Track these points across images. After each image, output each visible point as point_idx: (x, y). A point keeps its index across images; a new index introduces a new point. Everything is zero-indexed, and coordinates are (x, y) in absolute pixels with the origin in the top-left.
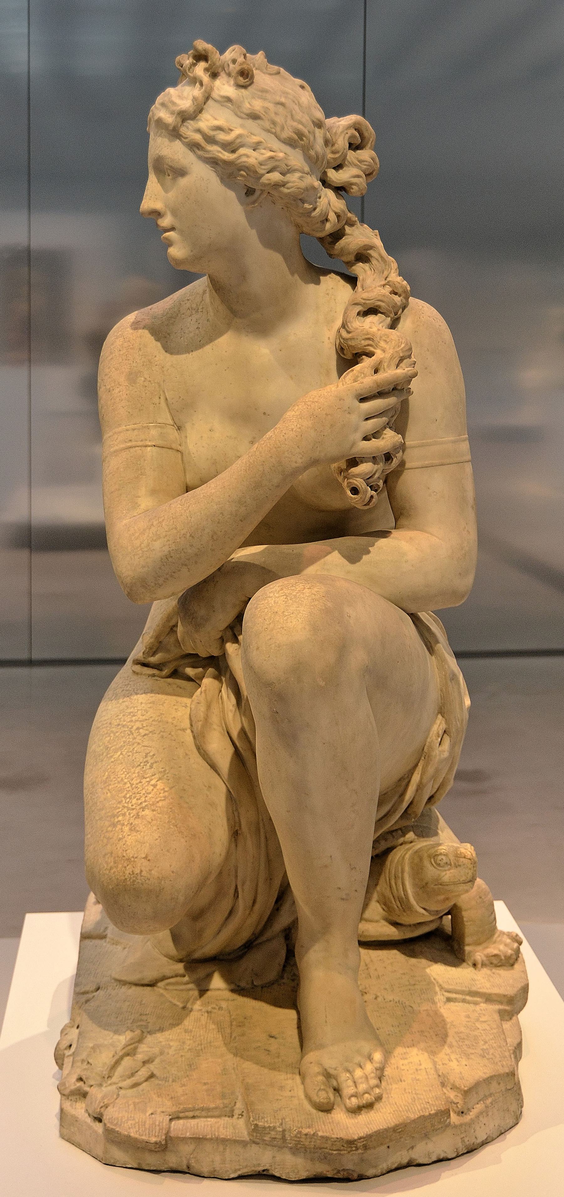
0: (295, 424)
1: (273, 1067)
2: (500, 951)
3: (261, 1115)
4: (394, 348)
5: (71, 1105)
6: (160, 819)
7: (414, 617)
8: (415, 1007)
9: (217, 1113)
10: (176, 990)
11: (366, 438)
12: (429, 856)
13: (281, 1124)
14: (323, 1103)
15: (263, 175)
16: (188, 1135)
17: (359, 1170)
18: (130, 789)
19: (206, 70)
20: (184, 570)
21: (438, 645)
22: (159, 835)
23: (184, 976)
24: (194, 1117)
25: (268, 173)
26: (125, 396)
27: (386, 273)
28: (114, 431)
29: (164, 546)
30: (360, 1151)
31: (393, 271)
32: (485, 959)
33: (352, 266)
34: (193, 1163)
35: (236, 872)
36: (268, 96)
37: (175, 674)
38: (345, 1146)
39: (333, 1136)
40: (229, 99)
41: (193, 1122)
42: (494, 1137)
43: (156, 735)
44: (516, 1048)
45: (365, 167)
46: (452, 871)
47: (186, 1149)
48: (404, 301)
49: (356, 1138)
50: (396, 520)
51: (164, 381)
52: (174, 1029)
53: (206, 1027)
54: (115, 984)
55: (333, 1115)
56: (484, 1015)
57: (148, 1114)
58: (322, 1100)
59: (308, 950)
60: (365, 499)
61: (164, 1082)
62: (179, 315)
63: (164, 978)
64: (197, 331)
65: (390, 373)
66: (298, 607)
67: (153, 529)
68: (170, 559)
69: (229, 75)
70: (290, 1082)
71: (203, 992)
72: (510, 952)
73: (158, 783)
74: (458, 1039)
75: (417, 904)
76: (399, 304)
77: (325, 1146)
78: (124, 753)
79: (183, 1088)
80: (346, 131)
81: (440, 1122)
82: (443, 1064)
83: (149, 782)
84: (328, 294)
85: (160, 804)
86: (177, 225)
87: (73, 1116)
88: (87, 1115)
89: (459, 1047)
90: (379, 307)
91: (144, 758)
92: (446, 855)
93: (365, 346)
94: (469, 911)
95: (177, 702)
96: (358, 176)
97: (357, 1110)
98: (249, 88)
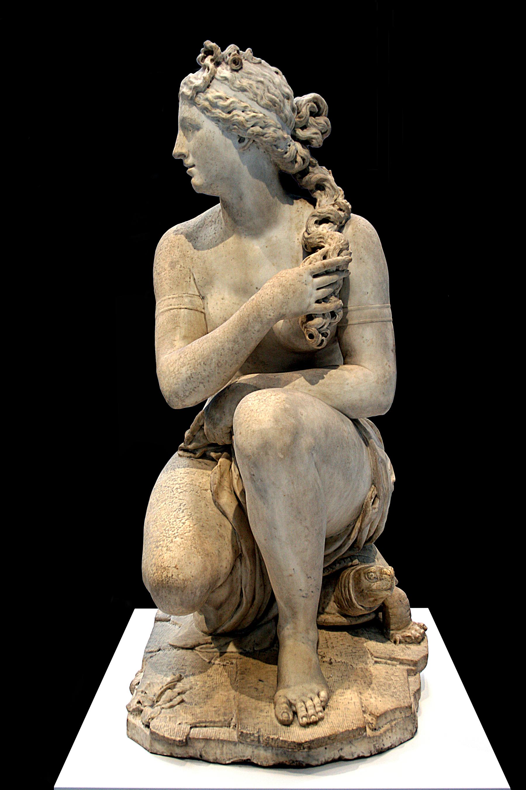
0: (269, 290)
1: (258, 698)
2: (412, 634)
3: (246, 726)
4: (336, 243)
5: (134, 718)
6: (186, 543)
7: (355, 422)
8: (354, 666)
9: (220, 724)
10: (206, 652)
11: (318, 302)
12: (365, 573)
13: (258, 732)
14: (285, 721)
15: (249, 128)
16: (201, 737)
17: (306, 761)
18: (169, 525)
19: (212, 60)
20: (201, 386)
21: (372, 440)
22: (184, 553)
23: (211, 644)
24: (205, 727)
25: (252, 126)
26: (168, 276)
27: (335, 197)
28: (161, 299)
29: (188, 370)
30: (306, 750)
31: (340, 196)
32: (401, 638)
33: (313, 193)
34: (203, 754)
35: (241, 580)
36: (253, 77)
37: (204, 456)
38: (297, 746)
39: (289, 740)
40: (226, 79)
41: (205, 729)
42: (396, 745)
43: (187, 493)
44: (415, 692)
45: (321, 127)
46: (378, 582)
47: (200, 745)
48: (347, 215)
49: (303, 741)
50: (344, 358)
51: (193, 267)
52: (201, 675)
53: (221, 674)
54: (170, 647)
55: (290, 727)
56: (397, 672)
57: (177, 724)
58: (284, 718)
59: (283, 629)
60: (317, 342)
61: (189, 705)
62: (204, 226)
63: (199, 645)
64: (214, 236)
65: (333, 259)
66: (267, 407)
67: (182, 360)
68: (192, 379)
69: (227, 63)
70: (267, 707)
71: (222, 654)
72: (418, 634)
73: (186, 521)
74: (377, 685)
75: (357, 603)
76: (342, 216)
77: (284, 746)
78: (167, 503)
79: (201, 709)
80: (307, 104)
81: (359, 734)
82: (366, 700)
83: (181, 521)
84: (298, 211)
85: (186, 534)
86: (196, 163)
87: (133, 724)
88: (142, 723)
89: (378, 690)
90: (329, 217)
91: (178, 506)
92: (375, 572)
93: (319, 242)
94: (393, 609)
95: (203, 473)
96: (316, 133)
97: (308, 725)
98: (240, 71)
